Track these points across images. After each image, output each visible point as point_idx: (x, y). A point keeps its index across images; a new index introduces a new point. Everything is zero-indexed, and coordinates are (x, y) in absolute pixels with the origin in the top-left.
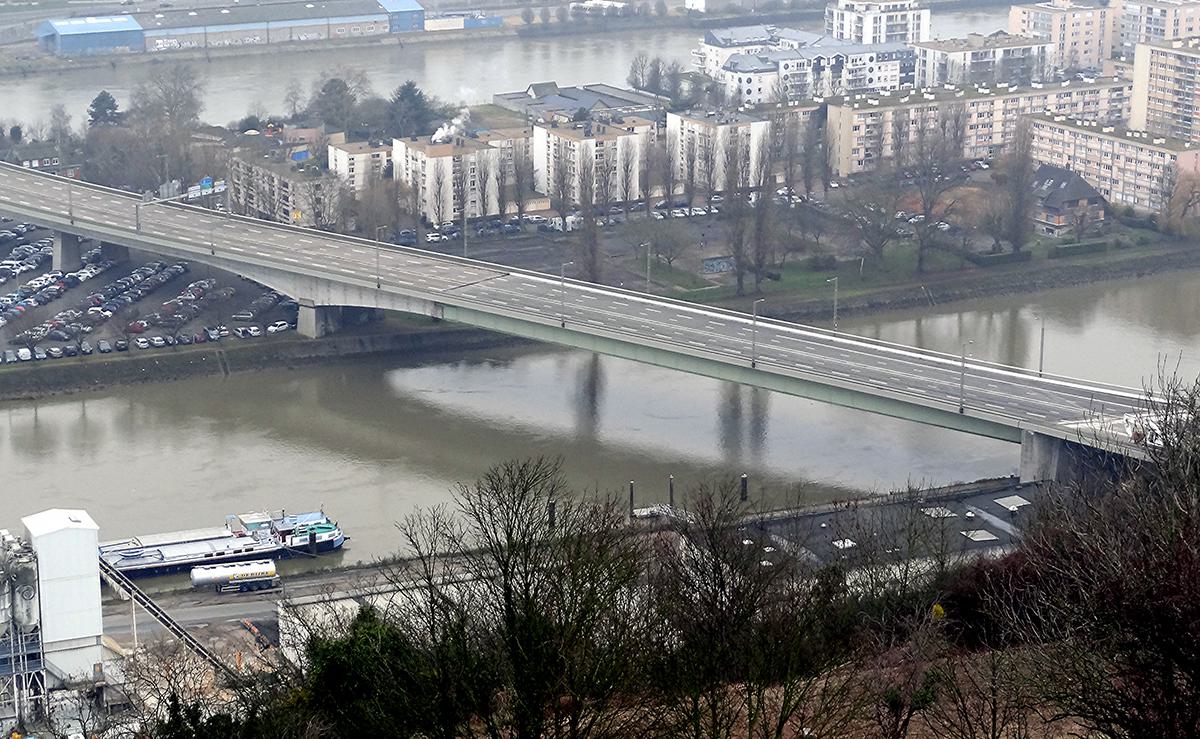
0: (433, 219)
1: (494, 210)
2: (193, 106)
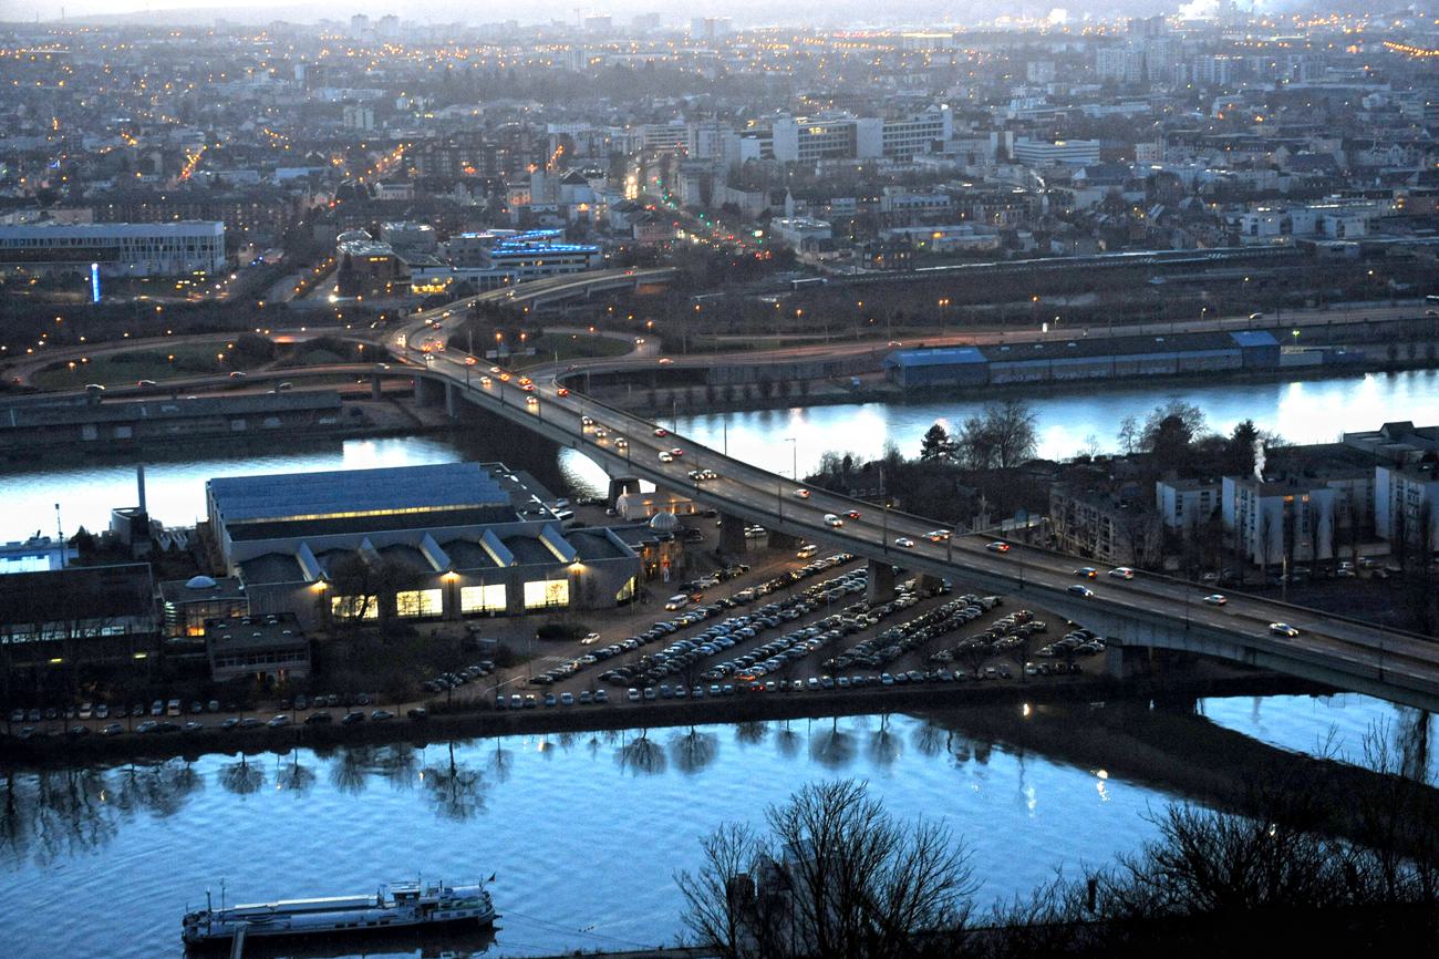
0: (1259, 560)
1: (1326, 552)
2: (1024, 435)
